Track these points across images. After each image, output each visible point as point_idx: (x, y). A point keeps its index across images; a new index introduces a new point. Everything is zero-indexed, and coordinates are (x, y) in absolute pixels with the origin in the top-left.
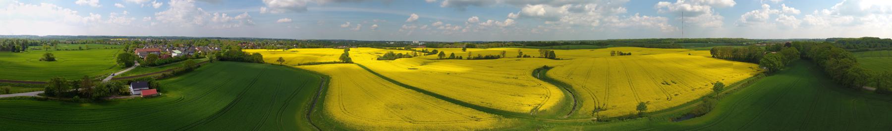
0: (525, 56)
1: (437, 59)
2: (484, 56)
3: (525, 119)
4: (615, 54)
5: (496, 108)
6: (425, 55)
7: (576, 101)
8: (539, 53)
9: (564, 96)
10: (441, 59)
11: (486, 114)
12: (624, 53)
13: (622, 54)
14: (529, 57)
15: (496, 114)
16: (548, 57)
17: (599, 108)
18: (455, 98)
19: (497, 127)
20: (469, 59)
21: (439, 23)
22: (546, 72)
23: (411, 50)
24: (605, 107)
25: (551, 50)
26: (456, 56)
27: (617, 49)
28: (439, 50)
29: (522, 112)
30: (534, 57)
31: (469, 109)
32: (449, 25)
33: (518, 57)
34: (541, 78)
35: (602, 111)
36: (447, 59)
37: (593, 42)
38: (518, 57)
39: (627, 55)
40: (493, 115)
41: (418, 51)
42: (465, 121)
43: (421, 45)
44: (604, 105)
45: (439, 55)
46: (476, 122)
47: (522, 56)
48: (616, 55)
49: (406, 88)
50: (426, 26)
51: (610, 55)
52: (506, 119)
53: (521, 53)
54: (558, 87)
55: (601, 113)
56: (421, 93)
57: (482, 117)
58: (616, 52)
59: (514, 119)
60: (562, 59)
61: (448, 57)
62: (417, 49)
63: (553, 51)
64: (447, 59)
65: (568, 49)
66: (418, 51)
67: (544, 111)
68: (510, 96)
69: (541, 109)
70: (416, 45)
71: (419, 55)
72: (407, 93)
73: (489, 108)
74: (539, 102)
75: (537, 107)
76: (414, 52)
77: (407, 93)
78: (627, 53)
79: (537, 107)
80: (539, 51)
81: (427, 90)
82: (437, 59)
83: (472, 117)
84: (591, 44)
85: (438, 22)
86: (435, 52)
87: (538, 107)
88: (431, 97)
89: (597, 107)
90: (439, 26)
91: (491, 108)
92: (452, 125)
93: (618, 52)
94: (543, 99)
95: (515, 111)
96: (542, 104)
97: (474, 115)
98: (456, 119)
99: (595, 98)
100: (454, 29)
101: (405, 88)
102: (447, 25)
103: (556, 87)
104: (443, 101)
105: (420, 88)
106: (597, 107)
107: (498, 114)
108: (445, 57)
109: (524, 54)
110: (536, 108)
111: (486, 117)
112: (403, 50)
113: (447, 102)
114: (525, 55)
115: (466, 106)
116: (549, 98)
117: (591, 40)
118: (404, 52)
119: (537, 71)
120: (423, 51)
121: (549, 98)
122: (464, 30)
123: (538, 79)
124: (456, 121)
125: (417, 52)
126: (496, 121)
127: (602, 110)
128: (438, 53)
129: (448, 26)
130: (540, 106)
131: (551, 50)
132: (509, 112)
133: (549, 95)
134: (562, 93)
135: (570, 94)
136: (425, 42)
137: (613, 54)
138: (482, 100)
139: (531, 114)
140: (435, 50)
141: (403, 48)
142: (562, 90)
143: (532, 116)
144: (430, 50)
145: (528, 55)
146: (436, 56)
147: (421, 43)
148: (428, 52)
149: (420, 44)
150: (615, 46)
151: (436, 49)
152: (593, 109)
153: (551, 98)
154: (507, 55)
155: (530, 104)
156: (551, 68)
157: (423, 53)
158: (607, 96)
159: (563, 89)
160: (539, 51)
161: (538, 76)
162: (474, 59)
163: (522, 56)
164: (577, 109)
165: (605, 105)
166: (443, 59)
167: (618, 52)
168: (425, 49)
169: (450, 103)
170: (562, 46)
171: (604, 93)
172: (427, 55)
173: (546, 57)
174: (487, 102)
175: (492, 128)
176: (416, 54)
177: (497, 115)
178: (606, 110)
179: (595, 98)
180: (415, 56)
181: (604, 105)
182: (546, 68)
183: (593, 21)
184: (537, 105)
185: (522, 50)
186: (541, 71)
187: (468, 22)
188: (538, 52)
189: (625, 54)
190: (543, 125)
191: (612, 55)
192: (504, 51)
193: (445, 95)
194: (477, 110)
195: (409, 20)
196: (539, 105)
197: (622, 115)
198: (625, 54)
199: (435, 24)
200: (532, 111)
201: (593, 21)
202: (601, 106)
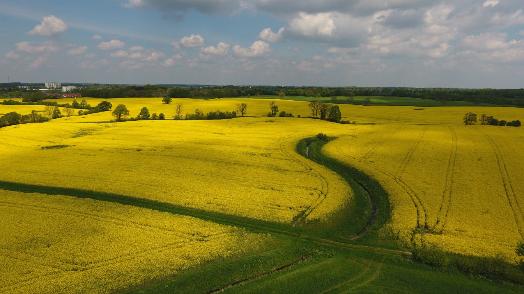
0: (283, 115)
1: (112, 122)
2: (206, 113)
3: (283, 235)
4: (475, 120)
5: (233, 213)
6: (80, 114)
7: (374, 208)
8: (310, 109)
9: (352, 194)
10: (119, 120)
11: (217, 225)
12: (499, 120)
13: (493, 122)
14: (290, 116)
15: (233, 224)
16: (327, 117)
17: (426, 227)
18: (159, 200)
19: (237, 252)
20: (177, 118)
21: (114, 43)
22: (322, 146)
23: (43, 104)
24: (439, 227)
25: (334, 105)
26: (151, 114)
27: (479, 111)
28: (115, 103)
29: (277, 221)
30: (299, 116)
31: (186, 220)
32: (139, 48)
33: (270, 115)
34: (310, 157)
35: (433, 235)
36: (132, 119)
37: (416, 90)
38: (270, 115)
39: (510, 124)
40: (230, 226)
41: (63, 106)
42: (182, 245)
43: (67, 92)
44: (438, 222)
45: (115, 113)
46: (200, 243)
47: (278, 113)
48: (479, 122)
49: (49, 194)
50: (84, 48)
51: (462, 121)
52: (251, 235)
53: (275, 108)
54: (343, 176)
55: (430, 238)
56: (87, 199)
57: (211, 233)
58: (478, 118)
59: (264, 234)
60: (354, 123)
61: (135, 116)
62: (60, 102)
63: (337, 107)
64: (132, 119)
65: (367, 103)
66: (63, 106)
67: (316, 222)
68: (257, 190)
69: (311, 217)
70: (56, 94)
71: (65, 114)
72: (52, 206)
73: (221, 214)
74: (308, 203)
75: (304, 212)
76: (52, 109)
77: (52, 206)
78: (509, 120)
79: (304, 212)
80: (309, 105)
81: (98, 190)
82: (112, 122)
83: (194, 235)
84: (409, 96)
85: (112, 42)
86: (104, 107)
87: (306, 213)
88: (110, 204)
89: (422, 223)
90: (116, 49)
91: (226, 212)
92: (159, 255)
93: (484, 116)
94: (314, 197)
95: (267, 219)
96: (312, 207)
97: (197, 230)
98: (166, 243)
99: (418, 204)
100: (149, 58)
101: (45, 195)
102: (134, 48)
103: (339, 177)
104: (136, 208)
105: (82, 188)
106: (422, 223)
107: (238, 225)
108: (129, 117)
109: (280, 110)
110: (302, 215)
111: (218, 232)
112: (18, 103)
113: (144, 210)
114: (284, 112)
115: (180, 214)
116: (325, 196)
117: (417, 86)
118: (24, 110)
119: (305, 143)
120: (76, 106)
121: (325, 196)
122: (169, 62)
123: (306, 158)
124: (166, 246)
125: (61, 109)
126: (234, 238)
127: (433, 232)
128: (113, 109)
129: (135, 52)
130: (309, 211)
131: (334, 105)
132: (256, 220)
133: (325, 190)
134: (349, 189)
135: (366, 192)
136: (76, 85)
137: (470, 120)
138: (208, 198)
139: (294, 226)
140: (105, 103)
141: (20, 100)
142: (350, 184)
143: (295, 230)
144: (94, 103)
145: (287, 112)
146: (108, 115)
147: (69, 88)
148: (88, 108)
149: (64, 89)
150: (476, 103)
151: (108, 100)
152: (414, 225)
153: (329, 196)
154: (248, 110)
155: (292, 206)
156: (333, 138)
157: (77, 111)
158: (445, 206)
159: (353, 181)
160: (309, 105)
161: (307, 153)
162: (187, 119)
163: (278, 113)
164: (375, 225)
165: (441, 224)
166: (125, 120)
167: (484, 116)
168: (79, 101)
169: (149, 210)
170: (357, 99)
171: (441, 198)
172: (86, 113)
173: (323, 118)
174: (218, 201)
175: (229, 253)
176: (59, 112)
177: (235, 228)
178: (440, 233)
179: (418, 204)
180: (55, 117)
181: (438, 222)
182: (322, 139)
183: (436, 46)
184: (304, 209)
185: (278, 101)
186: (313, 144)
187: (181, 46)
188: (308, 108)
189: (503, 123)
190: (314, 250)
191: (466, 124)
192: (242, 104)
193: (139, 196)
194: (201, 218)
195: (38, 28)
196: (308, 208)
197: (477, 254)
198: (503, 123)
199: (106, 45)
200: (295, 219)
201: (436, 46)
202: (431, 223)
